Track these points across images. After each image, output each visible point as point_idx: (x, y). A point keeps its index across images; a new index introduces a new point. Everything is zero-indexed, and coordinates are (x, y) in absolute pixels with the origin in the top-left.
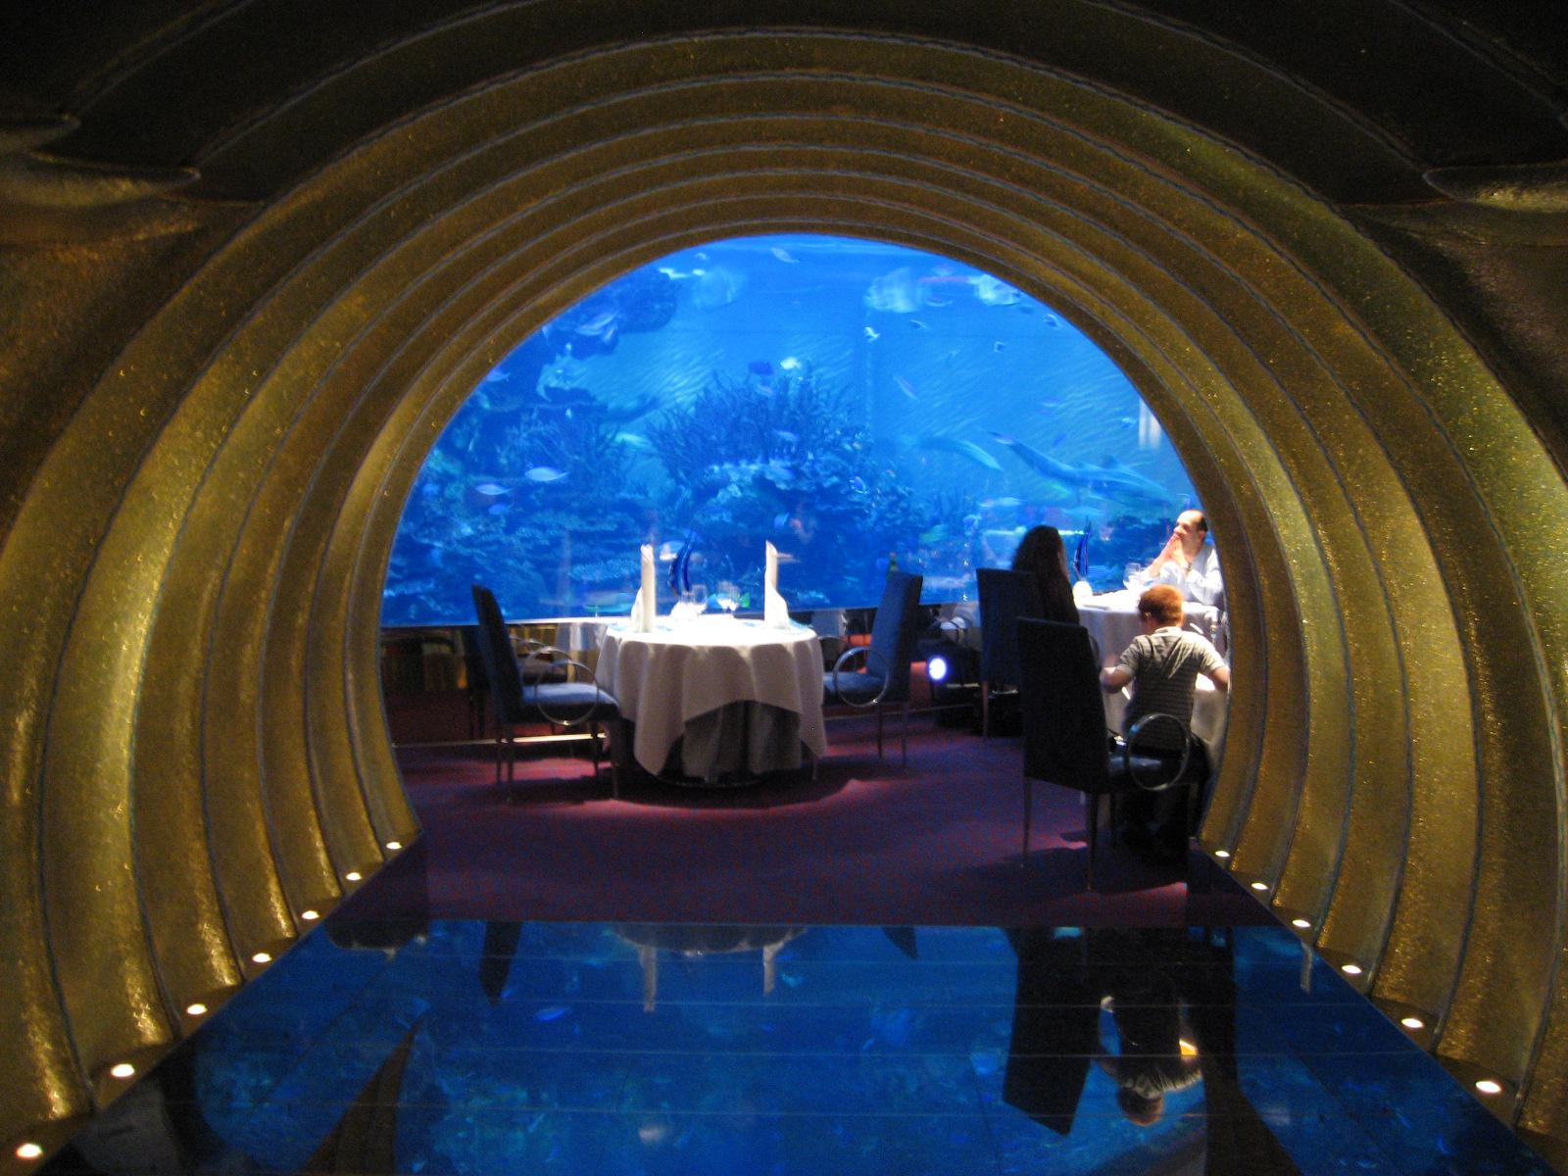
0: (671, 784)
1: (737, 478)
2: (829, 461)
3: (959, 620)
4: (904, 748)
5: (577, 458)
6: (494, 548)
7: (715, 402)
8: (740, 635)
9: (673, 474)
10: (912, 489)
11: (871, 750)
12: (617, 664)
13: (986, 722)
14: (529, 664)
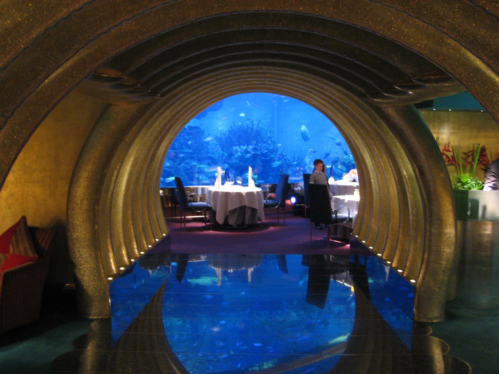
0: (226, 226)
1: (239, 150)
2: (265, 146)
3: (299, 188)
4: (284, 220)
5: (196, 145)
6: (176, 169)
7: (234, 130)
8: (243, 190)
9: (223, 150)
10: (287, 154)
11: (276, 221)
12: (212, 197)
13: (306, 214)
14: (189, 198)
